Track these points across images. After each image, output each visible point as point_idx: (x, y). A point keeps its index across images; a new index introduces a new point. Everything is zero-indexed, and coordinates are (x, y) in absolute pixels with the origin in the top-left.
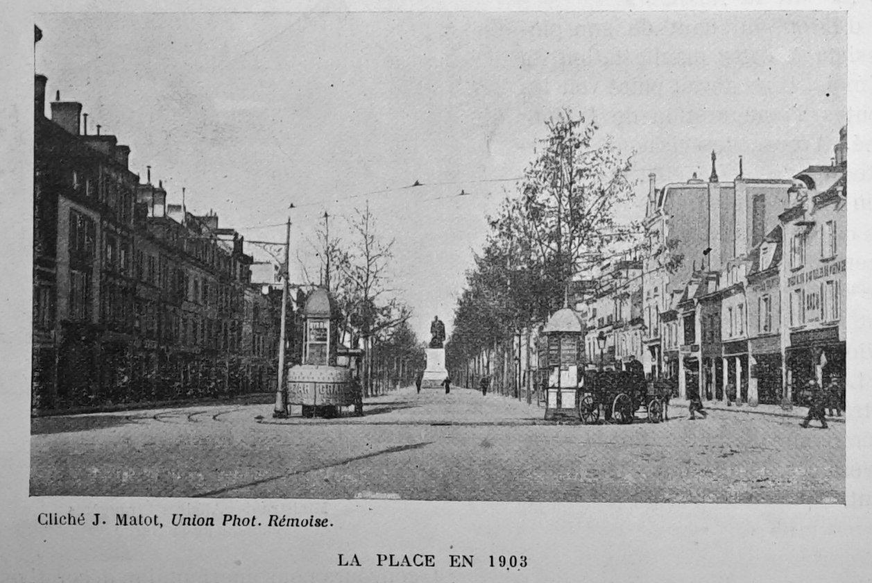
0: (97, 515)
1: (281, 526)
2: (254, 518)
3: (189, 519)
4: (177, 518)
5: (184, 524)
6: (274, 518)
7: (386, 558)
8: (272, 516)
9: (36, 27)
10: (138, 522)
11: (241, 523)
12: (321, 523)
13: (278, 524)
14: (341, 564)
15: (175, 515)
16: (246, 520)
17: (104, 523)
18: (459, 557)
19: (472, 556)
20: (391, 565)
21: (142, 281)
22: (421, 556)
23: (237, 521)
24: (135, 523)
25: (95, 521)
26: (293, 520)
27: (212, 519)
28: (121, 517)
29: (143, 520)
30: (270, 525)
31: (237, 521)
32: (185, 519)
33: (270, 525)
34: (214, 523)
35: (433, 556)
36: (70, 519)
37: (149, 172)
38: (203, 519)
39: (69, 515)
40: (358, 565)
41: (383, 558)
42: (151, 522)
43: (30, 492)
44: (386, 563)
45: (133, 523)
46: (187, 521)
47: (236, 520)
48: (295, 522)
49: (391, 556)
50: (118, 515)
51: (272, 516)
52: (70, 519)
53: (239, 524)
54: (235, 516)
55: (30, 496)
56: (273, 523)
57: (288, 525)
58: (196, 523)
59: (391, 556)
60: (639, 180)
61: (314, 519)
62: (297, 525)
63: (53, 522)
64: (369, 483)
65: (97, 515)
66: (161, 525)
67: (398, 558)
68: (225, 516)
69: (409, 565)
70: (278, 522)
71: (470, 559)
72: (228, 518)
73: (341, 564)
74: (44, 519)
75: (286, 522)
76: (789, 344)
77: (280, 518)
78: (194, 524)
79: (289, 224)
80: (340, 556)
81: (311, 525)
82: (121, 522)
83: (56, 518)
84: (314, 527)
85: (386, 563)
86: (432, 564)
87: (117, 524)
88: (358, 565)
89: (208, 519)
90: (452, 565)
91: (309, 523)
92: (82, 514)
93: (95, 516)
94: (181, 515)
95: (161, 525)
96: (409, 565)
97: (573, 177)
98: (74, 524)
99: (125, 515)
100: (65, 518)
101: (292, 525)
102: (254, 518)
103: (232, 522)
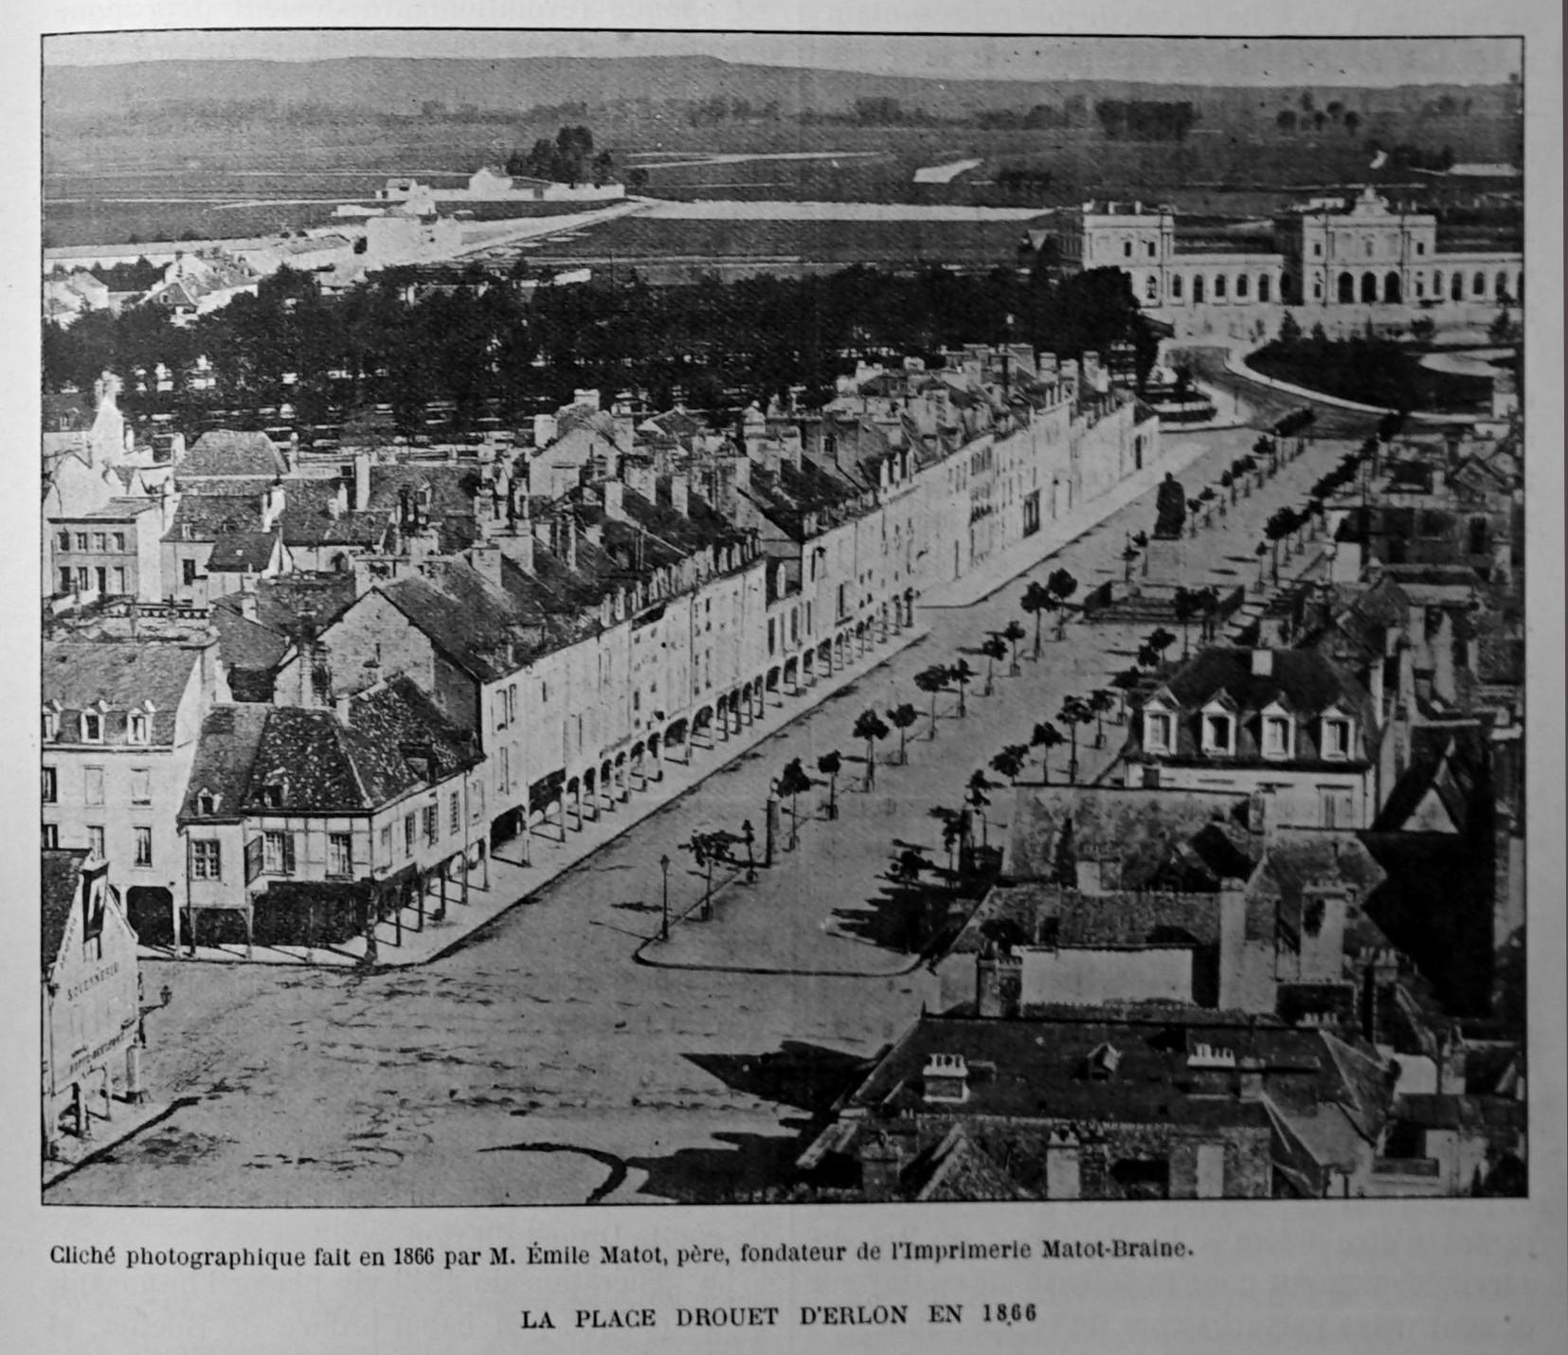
40: (550, 1326)
44: (588, 1323)
50: (605, 1249)
67: (605, 1316)
73: (526, 1326)
74: (59, 1255)
80: (526, 1314)
85: (588, 1323)
88: (550, 1326)
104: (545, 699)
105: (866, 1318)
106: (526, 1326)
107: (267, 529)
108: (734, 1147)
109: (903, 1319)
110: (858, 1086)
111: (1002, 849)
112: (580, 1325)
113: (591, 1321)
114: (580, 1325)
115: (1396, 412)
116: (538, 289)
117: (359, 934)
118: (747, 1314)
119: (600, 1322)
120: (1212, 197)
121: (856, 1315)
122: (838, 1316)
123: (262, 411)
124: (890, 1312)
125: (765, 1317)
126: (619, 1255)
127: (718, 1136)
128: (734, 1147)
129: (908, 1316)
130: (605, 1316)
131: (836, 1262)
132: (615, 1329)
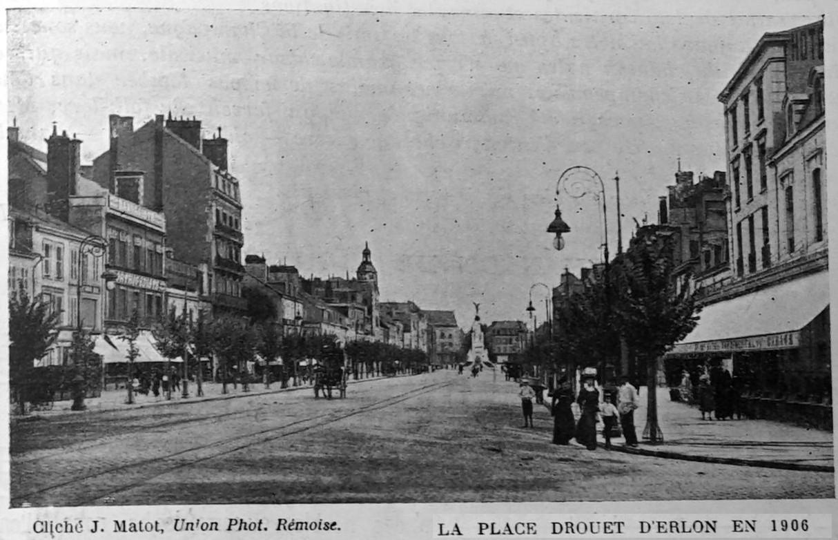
0: (96, 522)
1: (290, 529)
2: (260, 523)
3: (192, 524)
4: (179, 523)
5: (187, 529)
6: (283, 522)
7: (487, 526)
8: (280, 520)
10: (138, 528)
12: (329, 526)
13: (287, 528)
15: (177, 520)
16: (252, 528)
17: (102, 530)
20: (493, 533)
21: (711, 267)
22: (523, 524)
23: (243, 525)
24: (135, 530)
25: (94, 528)
26: (302, 523)
27: (216, 523)
28: (120, 523)
29: (143, 526)
30: (279, 529)
31: (69, 527)
32: (188, 524)
33: (279, 529)
34: (218, 528)
35: (534, 524)
36: (66, 526)
37: (679, 163)
39: (66, 522)
40: (460, 534)
41: (484, 526)
42: (152, 527)
43: (11, 502)
44: (487, 532)
45: (132, 529)
46: (190, 525)
47: (243, 525)
48: (304, 525)
49: (493, 524)
50: (117, 522)
51: (280, 520)
52: (66, 526)
54: (241, 520)
55: (10, 508)
56: (282, 527)
61: (323, 523)
62: (306, 529)
65: (96, 522)
66: (162, 531)
67: (500, 527)
68: (231, 520)
69: (511, 533)
70: (287, 525)
71: (752, 523)
72: (234, 522)
73: (441, 534)
74: (39, 528)
75: (294, 526)
76: (197, 317)
77: (289, 522)
78: (306, 529)
79: (617, 179)
80: (441, 525)
81: (320, 529)
82: (120, 528)
83: (51, 526)
84: (323, 531)
85: (487, 532)
87: (116, 531)
91: (318, 526)
92: (80, 522)
93: (94, 524)
94: (183, 520)
95: (162, 531)
96: (511, 533)
98: (72, 531)
99: (124, 522)
100: (61, 525)
101: (301, 529)
102: (260, 523)
103: (238, 526)
105: (687, 530)
106: (441, 534)
111: (613, 413)
113: (489, 530)
115: (36, 363)
118: (602, 525)
119: (496, 531)
120: (399, 383)
122: (667, 527)
123: (577, 417)
124: (705, 524)
125: (615, 528)
126: (127, 527)
127: (786, 451)
129: (757, 526)
131: (214, 531)
132: (508, 536)
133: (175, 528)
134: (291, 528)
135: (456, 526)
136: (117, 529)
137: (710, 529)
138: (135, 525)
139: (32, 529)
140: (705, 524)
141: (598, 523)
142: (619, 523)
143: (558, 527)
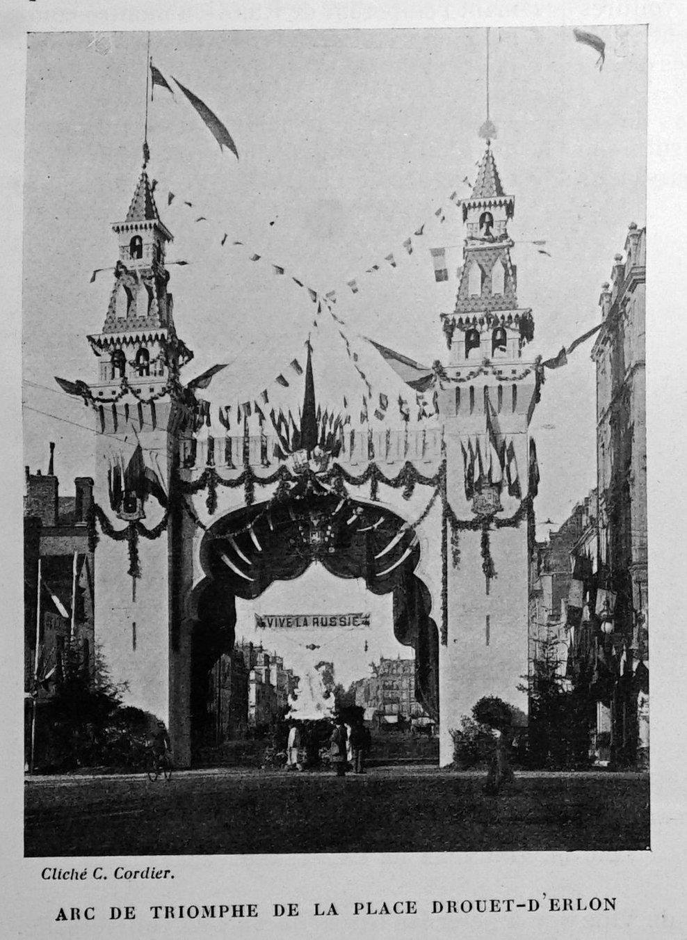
9: (56, 378)
11: (79, 877)
14: (317, 914)
18: (558, 900)
19: (614, 899)
20: (369, 912)
22: (50, 869)
23: (75, 875)
28: (209, 909)
31: (75, 875)
38: (131, 873)
49: (369, 904)
53: (77, 878)
57: (72, 878)
58: (154, 876)
59: (369, 904)
60: (223, 410)
62: (59, 878)
63: (57, 876)
64: (459, 839)
67: (376, 906)
69: (387, 912)
71: (612, 901)
73: (317, 914)
74: (48, 873)
78: (152, 877)
80: (317, 905)
82: (208, 913)
86: (296, 913)
88: (335, 913)
89: (136, 872)
90: (552, 909)
97: (439, 499)
104: (301, 285)
107: (345, 725)
108: (588, 593)
109: (613, 906)
110: (370, 530)
112: (356, 913)
114: (356, 913)
116: (306, 487)
117: (311, 561)
119: (373, 911)
121: (575, 905)
122: (561, 904)
124: (603, 902)
128: (588, 593)
130: (376, 906)
132: (384, 916)
133: (94, 875)
134: (159, 876)
135: (332, 906)
136: (205, 915)
137: (609, 906)
138: (478, 908)
139: (113, 873)
140: (603, 902)
141: (485, 901)
142: (156, 908)
143: (280, 909)
